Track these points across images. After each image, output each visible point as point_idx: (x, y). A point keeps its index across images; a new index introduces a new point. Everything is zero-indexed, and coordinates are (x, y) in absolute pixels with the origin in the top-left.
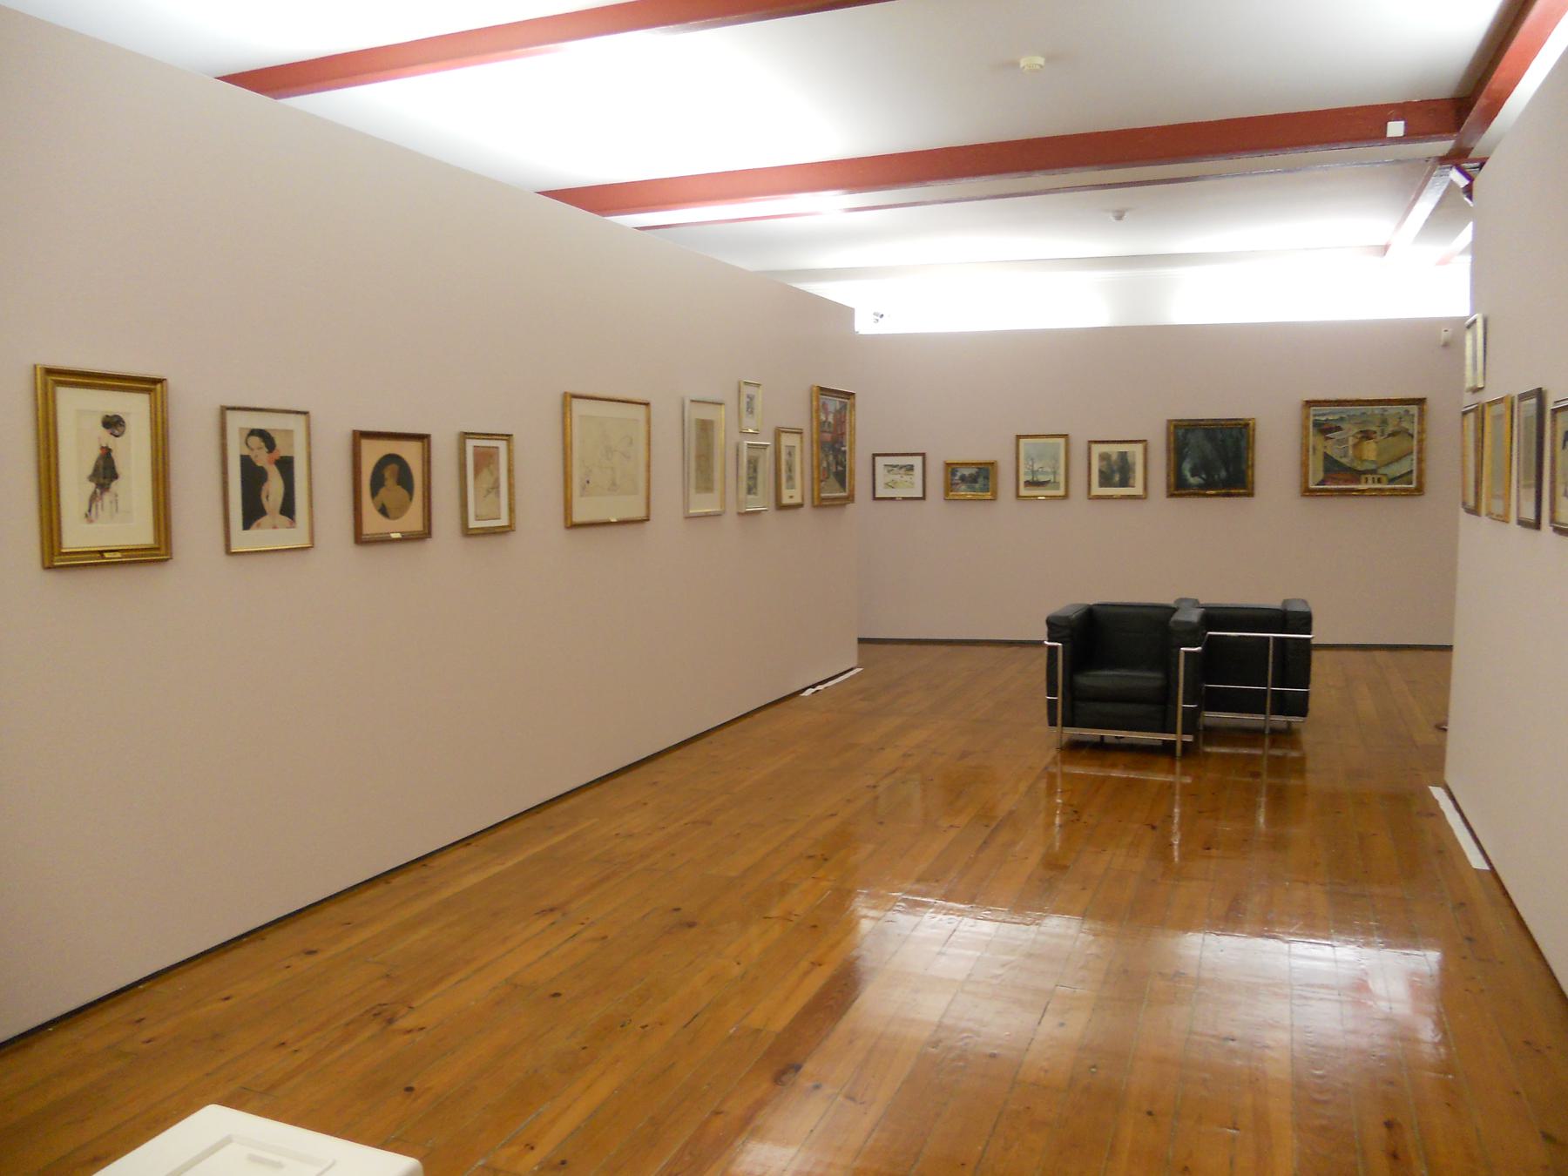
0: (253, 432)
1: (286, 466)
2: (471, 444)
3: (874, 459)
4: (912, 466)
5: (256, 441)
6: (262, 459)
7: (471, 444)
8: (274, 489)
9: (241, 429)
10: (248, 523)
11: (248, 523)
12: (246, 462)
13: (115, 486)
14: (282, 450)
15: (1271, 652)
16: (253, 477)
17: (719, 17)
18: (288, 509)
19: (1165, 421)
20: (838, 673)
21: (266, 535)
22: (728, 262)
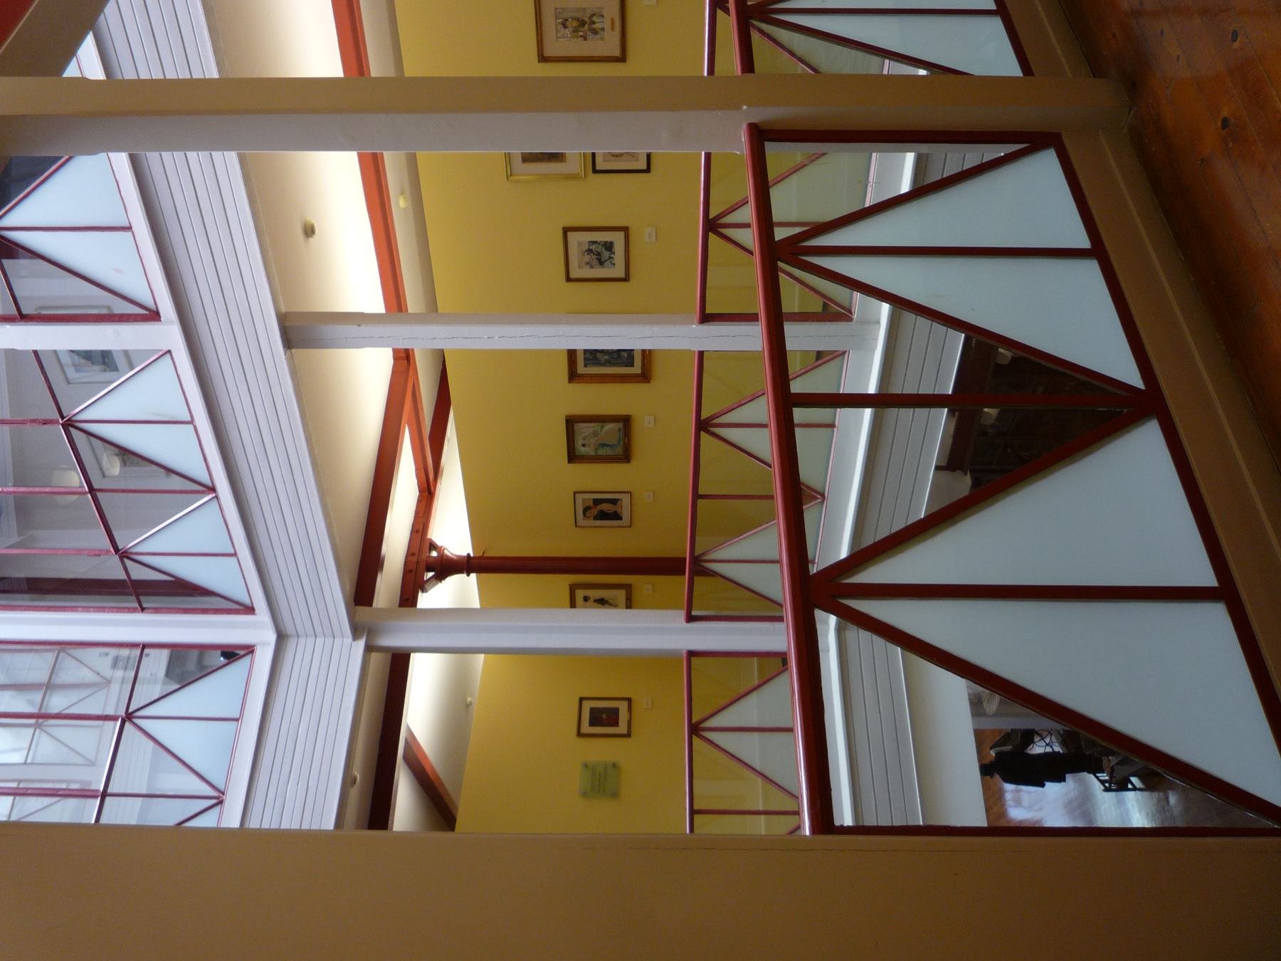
0: (584, 515)
1: (597, 502)
2: (619, 272)
3: (580, 527)
4: (611, 243)
5: (587, 514)
6: (595, 512)
7: (619, 272)
8: (606, 507)
9: (584, 519)
10: (620, 518)
11: (620, 518)
12: (595, 518)
13: (606, 599)
14: (591, 503)
15: (1257, 500)
16: (603, 516)
17: (44, 315)
18: (614, 502)
19: (571, 385)
20: (123, 14)
21: (625, 513)
22: (428, 433)
